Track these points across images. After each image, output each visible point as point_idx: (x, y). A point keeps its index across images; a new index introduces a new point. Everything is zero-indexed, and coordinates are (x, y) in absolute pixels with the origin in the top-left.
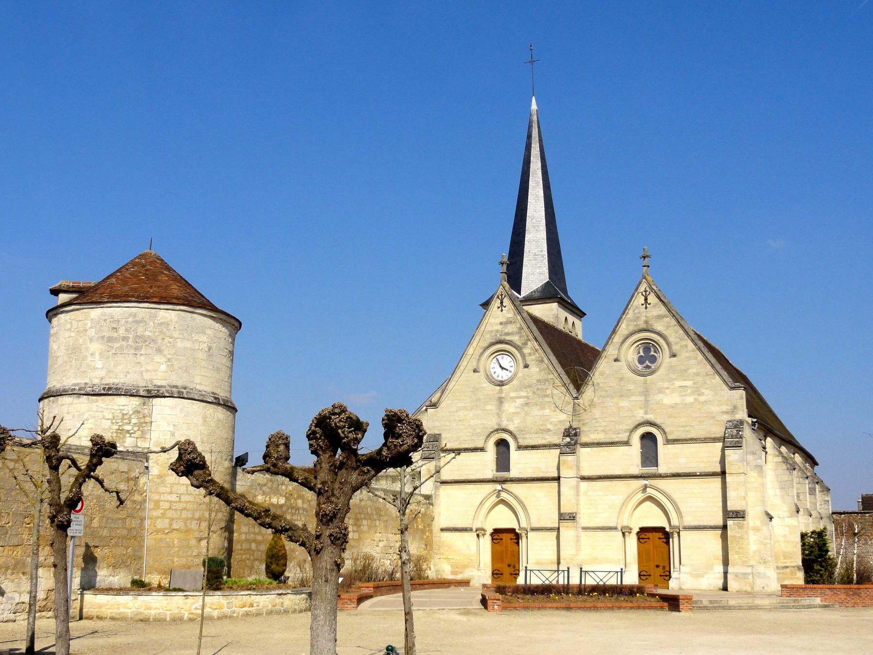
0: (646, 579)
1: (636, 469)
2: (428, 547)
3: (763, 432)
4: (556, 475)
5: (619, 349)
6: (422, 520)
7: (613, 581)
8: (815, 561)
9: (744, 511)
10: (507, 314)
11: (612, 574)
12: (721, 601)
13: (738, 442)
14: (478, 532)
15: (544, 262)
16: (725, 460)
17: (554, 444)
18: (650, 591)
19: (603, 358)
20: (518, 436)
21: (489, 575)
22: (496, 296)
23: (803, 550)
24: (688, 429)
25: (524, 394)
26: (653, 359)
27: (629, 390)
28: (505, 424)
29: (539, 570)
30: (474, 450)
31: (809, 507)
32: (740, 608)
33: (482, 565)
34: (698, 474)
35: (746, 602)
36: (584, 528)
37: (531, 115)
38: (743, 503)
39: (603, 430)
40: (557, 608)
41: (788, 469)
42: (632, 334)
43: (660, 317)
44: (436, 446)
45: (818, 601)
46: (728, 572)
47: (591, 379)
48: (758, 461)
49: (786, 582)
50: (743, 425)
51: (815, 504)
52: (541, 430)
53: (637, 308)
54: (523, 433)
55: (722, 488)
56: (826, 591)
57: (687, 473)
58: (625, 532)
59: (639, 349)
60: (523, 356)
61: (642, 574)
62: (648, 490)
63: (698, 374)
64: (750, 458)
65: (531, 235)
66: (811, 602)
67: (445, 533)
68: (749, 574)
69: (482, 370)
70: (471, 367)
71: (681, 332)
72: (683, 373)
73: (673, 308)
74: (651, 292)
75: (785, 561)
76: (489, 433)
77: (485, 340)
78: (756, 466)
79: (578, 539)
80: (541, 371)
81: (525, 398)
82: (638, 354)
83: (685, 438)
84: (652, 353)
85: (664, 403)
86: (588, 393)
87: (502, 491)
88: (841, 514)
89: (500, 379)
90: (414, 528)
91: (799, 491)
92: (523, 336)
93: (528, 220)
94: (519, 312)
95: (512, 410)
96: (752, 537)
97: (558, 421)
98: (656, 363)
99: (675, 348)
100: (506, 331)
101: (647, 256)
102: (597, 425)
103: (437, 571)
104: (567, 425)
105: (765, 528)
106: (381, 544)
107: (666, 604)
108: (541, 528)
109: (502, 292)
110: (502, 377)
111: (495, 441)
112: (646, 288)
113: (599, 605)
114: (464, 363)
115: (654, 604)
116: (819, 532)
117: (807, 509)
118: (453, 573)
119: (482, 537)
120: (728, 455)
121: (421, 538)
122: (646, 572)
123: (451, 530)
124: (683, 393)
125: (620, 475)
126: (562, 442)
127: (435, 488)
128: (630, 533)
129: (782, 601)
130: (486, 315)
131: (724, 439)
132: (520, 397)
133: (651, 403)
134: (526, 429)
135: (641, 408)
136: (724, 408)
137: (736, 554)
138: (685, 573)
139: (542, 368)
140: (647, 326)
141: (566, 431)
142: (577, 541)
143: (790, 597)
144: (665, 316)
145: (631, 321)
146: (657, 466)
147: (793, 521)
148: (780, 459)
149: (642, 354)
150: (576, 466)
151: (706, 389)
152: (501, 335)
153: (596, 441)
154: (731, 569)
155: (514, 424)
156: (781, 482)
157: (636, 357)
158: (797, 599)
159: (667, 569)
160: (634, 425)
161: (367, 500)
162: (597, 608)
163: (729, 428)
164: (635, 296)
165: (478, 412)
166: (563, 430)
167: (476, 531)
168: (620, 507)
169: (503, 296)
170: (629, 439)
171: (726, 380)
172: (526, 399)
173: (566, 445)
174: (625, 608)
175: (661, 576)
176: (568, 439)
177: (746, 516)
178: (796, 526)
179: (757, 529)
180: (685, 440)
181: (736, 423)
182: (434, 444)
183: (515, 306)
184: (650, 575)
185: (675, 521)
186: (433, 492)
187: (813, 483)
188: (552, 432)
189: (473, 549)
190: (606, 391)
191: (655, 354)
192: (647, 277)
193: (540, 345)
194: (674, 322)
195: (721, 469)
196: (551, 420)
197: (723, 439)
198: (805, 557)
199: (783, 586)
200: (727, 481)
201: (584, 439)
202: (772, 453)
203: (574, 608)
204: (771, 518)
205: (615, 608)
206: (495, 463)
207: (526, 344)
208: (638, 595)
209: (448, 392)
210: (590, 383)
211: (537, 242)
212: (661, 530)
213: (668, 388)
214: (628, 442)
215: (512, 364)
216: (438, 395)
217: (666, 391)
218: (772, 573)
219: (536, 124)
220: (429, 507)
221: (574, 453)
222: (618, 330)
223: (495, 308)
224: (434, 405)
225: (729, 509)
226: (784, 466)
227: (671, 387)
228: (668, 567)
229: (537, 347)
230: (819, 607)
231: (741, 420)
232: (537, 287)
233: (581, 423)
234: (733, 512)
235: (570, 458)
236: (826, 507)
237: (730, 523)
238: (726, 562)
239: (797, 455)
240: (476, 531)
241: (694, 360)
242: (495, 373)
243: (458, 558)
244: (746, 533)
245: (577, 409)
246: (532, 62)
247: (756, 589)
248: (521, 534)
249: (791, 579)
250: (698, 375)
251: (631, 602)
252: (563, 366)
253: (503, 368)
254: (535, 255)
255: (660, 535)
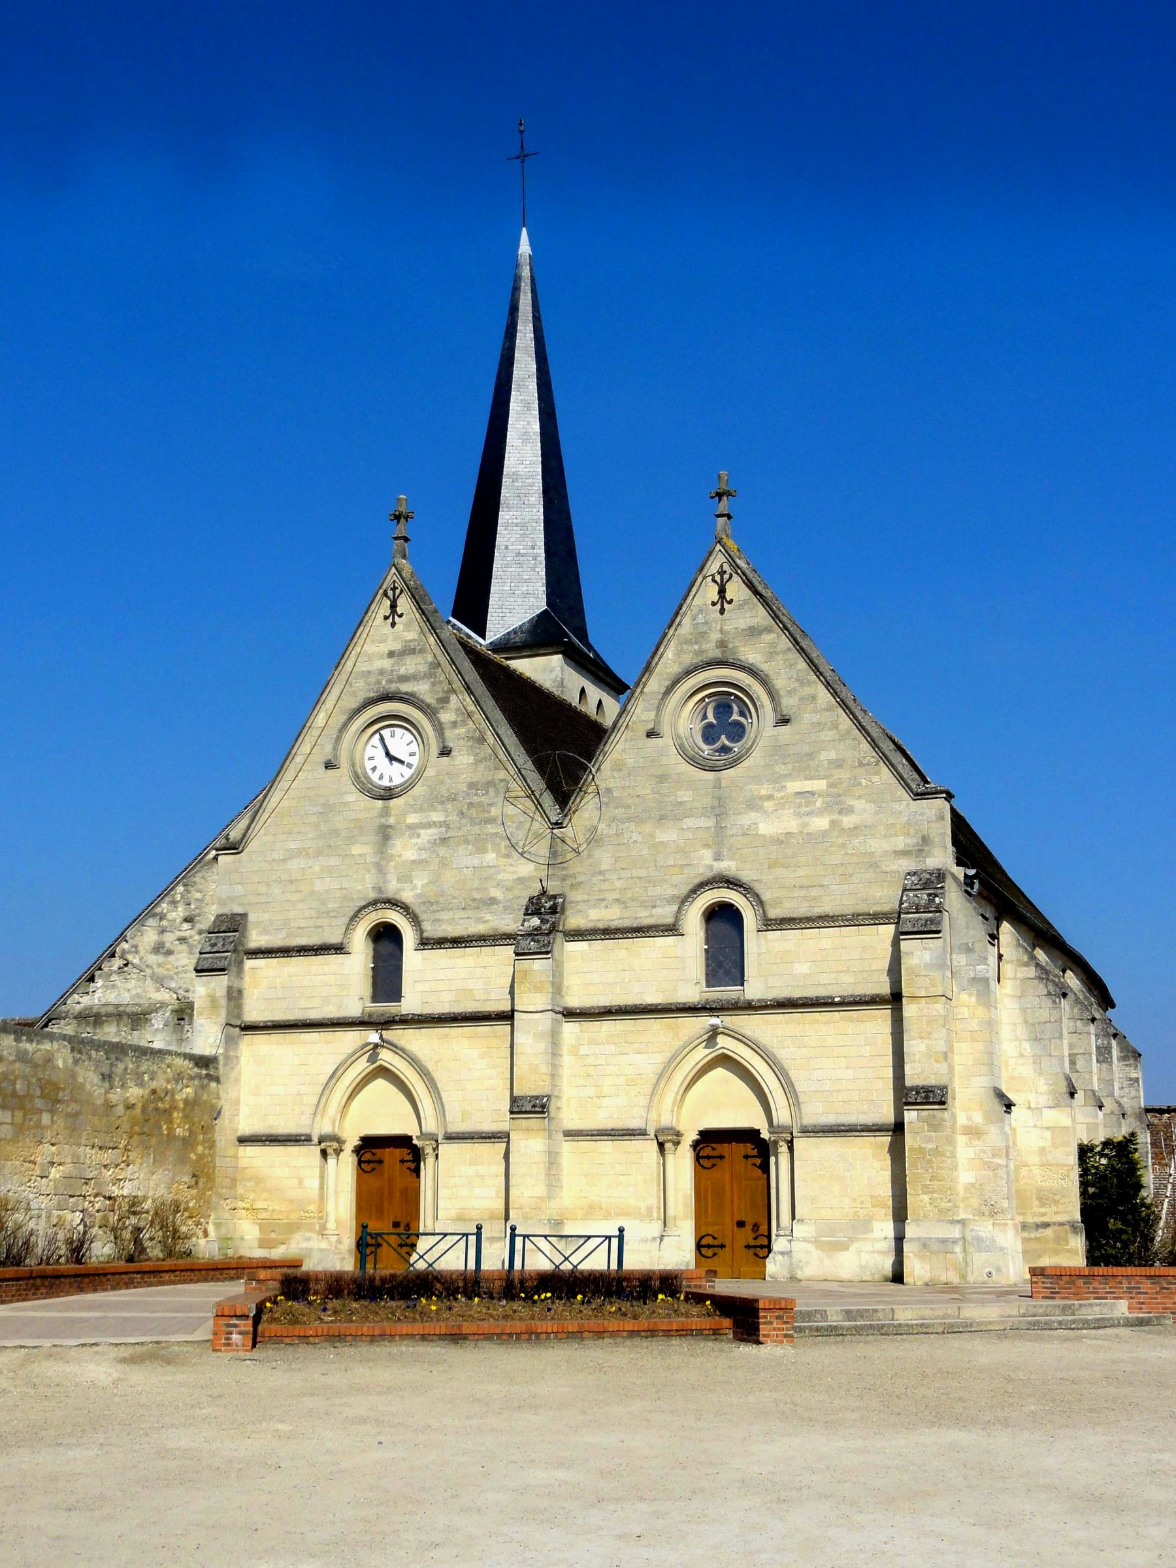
0: (715, 1254)
1: (693, 990)
2: (202, 1181)
3: (993, 909)
4: (506, 1007)
5: (658, 707)
6: (186, 1116)
7: (597, 1261)
8: (1112, 1212)
9: (943, 1089)
10: (405, 634)
11: (450, 1240)
12: (875, 1311)
13: (932, 921)
14: (323, 1145)
15: (536, 569)
16: (900, 964)
17: (504, 935)
18: (696, 1286)
19: (623, 728)
20: (422, 917)
21: (346, 1247)
22: (381, 591)
23: (1084, 1184)
24: (815, 892)
25: (436, 817)
26: (738, 732)
27: (681, 803)
28: (393, 888)
29: (545, 1237)
30: (322, 949)
31: (1096, 1088)
32: (923, 1330)
33: (331, 1225)
34: (837, 999)
35: (940, 1313)
36: (570, 1134)
37: (517, 265)
38: (942, 1068)
39: (617, 900)
40: (424, 1338)
41: (1049, 994)
42: (688, 673)
43: (753, 632)
44: (232, 942)
45: (1121, 1308)
46: (904, 1238)
47: (593, 779)
48: (979, 968)
49: (1045, 1262)
50: (943, 882)
51: (1111, 1082)
52: (474, 900)
53: (701, 611)
54: (434, 907)
55: (892, 1034)
56: (1141, 1283)
57: (811, 999)
58: (665, 1141)
59: (706, 708)
60: (439, 728)
61: (704, 1242)
62: (722, 1041)
63: (839, 764)
64: (960, 960)
65: (511, 513)
66: (1105, 1311)
67: (248, 1148)
68: (955, 1242)
69: (344, 762)
70: (320, 756)
71: (802, 665)
72: (805, 765)
73: (784, 612)
74: (734, 575)
75: (1043, 1210)
76: (356, 909)
77: (354, 694)
78: (974, 979)
79: (553, 1160)
80: (478, 762)
81: (441, 827)
82: (702, 720)
83: (809, 914)
84: (735, 717)
85: (759, 832)
86: (586, 810)
87: (383, 1046)
88: (1161, 1111)
89: (385, 783)
90: (162, 1135)
91: (1075, 1051)
92: (440, 682)
93: (506, 481)
94: (433, 628)
95: (410, 855)
96: (965, 1151)
97: (514, 880)
98: (744, 740)
99: (788, 703)
100: (402, 671)
101: (728, 494)
102: (605, 886)
103: (226, 1240)
104: (535, 889)
105: (993, 1130)
106: (54, 1173)
107: (727, 1322)
108: (469, 1133)
109: (394, 582)
110: (391, 780)
111: (366, 932)
112: (721, 566)
113: (542, 1326)
114: (304, 747)
115: (695, 1322)
116: (1120, 1143)
117: (1093, 1091)
118: (264, 1243)
119: (334, 1156)
120: (907, 953)
121: (183, 1160)
122: (715, 1238)
123: (261, 1141)
124: (804, 809)
125: (657, 1005)
126: (521, 928)
127: (226, 1042)
128: (677, 1143)
129: (1032, 1311)
130: (358, 635)
131: (900, 913)
132: (429, 825)
133: (729, 832)
134: (441, 900)
135: (706, 846)
136: (901, 842)
137: (925, 1193)
138: (805, 1240)
139: (482, 755)
140: (724, 652)
141: (532, 903)
142: (551, 1164)
143: (1053, 1298)
144: (768, 630)
145: (688, 642)
146: (742, 985)
147: (1060, 1117)
148: (1031, 972)
149: (711, 718)
150: (553, 984)
151: (859, 797)
152: (390, 681)
153: (601, 925)
154: (910, 1231)
155: (415, 888)
156: (1033, 1025)
157: (698, 726)
158: (1070, 1306)
159: (763, 1229)
160: (690, 887)
161: (15, 1061)
162: (538, 1335)
163: (910, 890)
164: (697, 584)
165: (333, 861)
166: (525, 901)
167: (320, 1143)
168: (655, 1082)
169: (398, 592)
170: (677, 919)
171: (905, 776)
172: (443, 829)
173: (529, 935)
174: (614, 1334)
175: (748, 1247)
176: (535, 921)
177: (950, 1100)
178: (1066, 1128)
179: (974, 1132)
180: (809, 919)
181: (928, 876)
182: (229, 937)
183: (423, 612)
184: (722, 1246)
185: (782, 1115)
186: (221, 1051)
187: (1105, 1036)
188: (501, 906)
189: (313, 1184)
190: (627, 807)
191: (742, 720)
192: (725, 540)
193: (477, 702)
194: (785, 642)
195: (891, 988)
196: (500, 877)
197: (895, 917)
198: (1089, 1202)
199: (1034, 1272)
200: (905, 1014)
201: (573, 920)
202: (1014, 958)
203: (471, 1337)
204: (1009, 1106)
205: (586, 1334)
206: (370, 980)
207: (445, 700)
208: (660, 1296)
209: (266, 815)
210: (591, 789)
211: (523, 526)
212: (750, 1135)
213: (770, 797)
214: (674, 925)
215: (414, 747)
216: (243, 824)
217: (766, 804)
218: (1009, 1239)
219: (529, 284)
220: (208, 1085)
221: (547, 953)
222: (657, 664)
223: (379, 619)
224: (234, 847)
225: (909, 1082)
226: (1042, 989)
227: (776, 794)
228: (766, 1227)
229: (472, 707)
230: (1125, 1325)
231: (938, 870)
232: (520, 623)
233: (568, 882)
234: (917, 1090)
235: (538, 965)
236: (1133, 1093)
237: (910, 1116)
238: (900, 1214)
239: (1069, 973)
240: (320, 1143)
241: (831, 729)
242: (374, 769)
243: (277, 1207)
244: (951, 1141)
245: (560, 849)
246: (522, 157)
247: (971, 1279)
248: (423, 1148)
249: (1057, 1252)
250: (840, 766)
251: (635, 1317)
252: (531, 751)
253: (392, 758)
254: (519, 554)
255: (749, 1148)
